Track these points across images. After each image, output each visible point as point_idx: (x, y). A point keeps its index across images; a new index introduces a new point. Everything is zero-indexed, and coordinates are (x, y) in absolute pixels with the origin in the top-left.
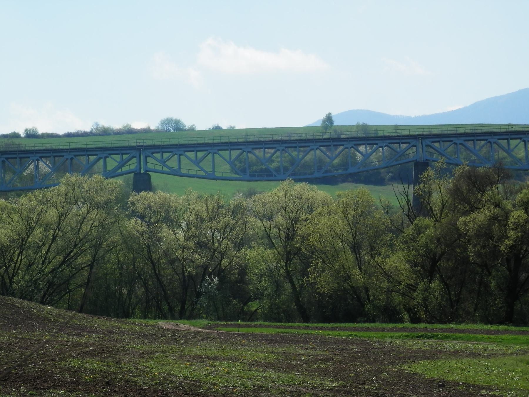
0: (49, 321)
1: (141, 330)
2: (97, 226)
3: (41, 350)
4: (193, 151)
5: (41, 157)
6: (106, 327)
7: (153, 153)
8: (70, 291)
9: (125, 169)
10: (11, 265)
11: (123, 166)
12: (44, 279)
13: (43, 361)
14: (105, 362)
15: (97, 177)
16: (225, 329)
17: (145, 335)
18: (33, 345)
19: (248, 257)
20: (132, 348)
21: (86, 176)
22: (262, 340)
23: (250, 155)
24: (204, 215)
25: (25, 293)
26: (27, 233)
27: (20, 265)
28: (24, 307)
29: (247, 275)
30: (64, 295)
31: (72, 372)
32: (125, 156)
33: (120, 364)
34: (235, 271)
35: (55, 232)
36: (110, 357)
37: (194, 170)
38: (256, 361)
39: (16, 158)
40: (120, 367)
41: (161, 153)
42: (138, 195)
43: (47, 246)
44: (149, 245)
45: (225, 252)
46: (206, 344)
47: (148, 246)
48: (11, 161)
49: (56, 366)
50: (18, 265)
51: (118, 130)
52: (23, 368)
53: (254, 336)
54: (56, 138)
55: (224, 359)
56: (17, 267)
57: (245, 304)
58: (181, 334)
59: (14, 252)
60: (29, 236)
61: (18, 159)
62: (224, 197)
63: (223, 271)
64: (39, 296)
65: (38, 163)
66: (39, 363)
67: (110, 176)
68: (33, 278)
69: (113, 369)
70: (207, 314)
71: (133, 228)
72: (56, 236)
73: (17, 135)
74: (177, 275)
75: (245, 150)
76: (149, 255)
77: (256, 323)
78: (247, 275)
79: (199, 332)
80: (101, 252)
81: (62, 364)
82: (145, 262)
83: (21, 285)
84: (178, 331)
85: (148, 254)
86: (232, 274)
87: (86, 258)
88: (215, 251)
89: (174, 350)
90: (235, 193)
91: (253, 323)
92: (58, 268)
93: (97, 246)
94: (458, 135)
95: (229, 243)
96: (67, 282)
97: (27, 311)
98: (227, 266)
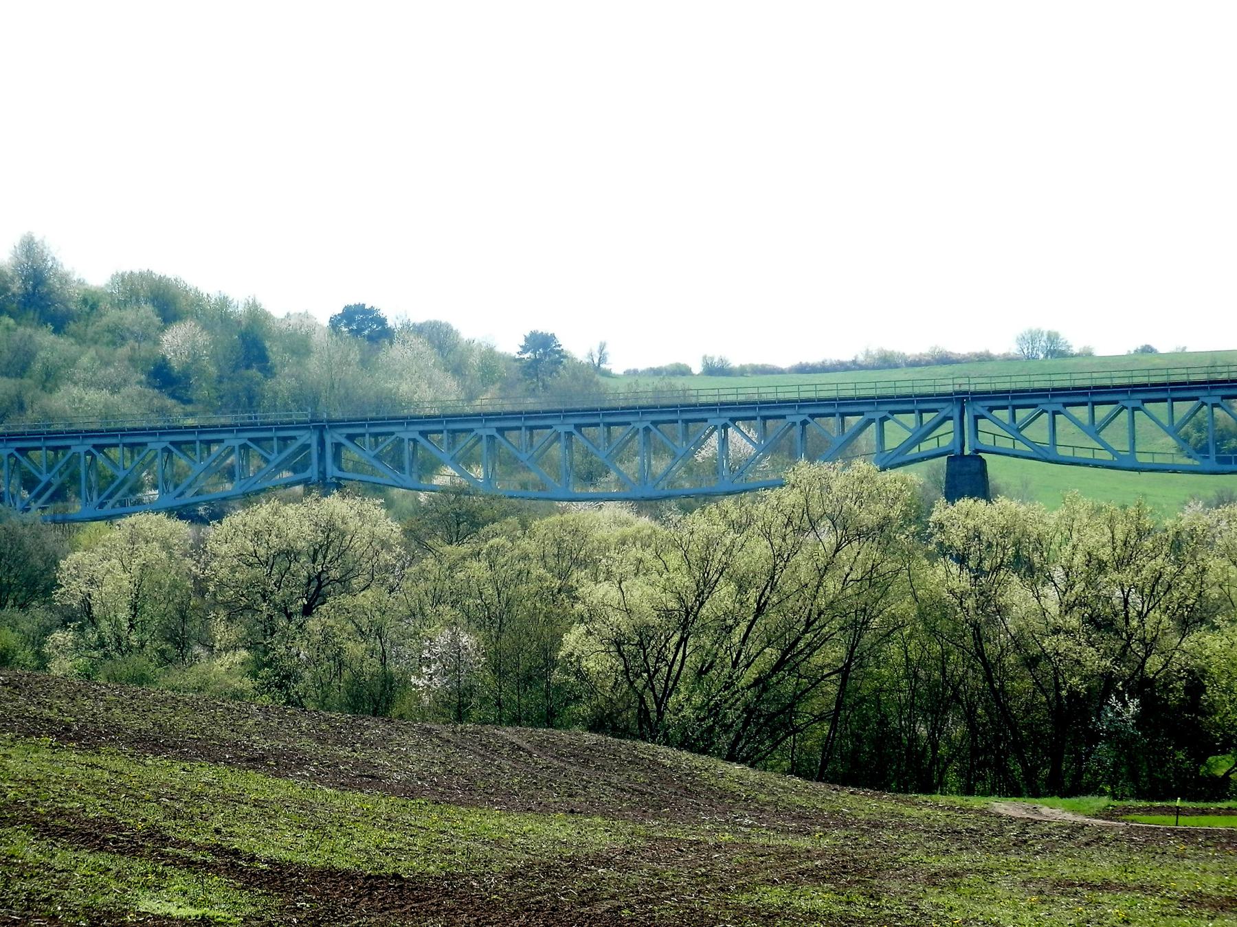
0: (736, 797)
1: (948, 820)
2: (858, 581)
3: (700, 866)
4: (1085, 404)
5: (734, 420)
6: (867, 814)
7: (991, 409)
8: (797, 730)
9: (928, 446)
10: (659, 668)
11: (923, 438)
12: (736, 701)
13: (699, 892)
14: (843, 895)
15: (862, 466)
16: (1146, 818)
17: (955, 832)
18: (684, 854)
19: (1208, 653)
20: (913, 862)
21: (839, 464)
22: (1228, 843)
23: (1216, 410)
24: (1105, 554)
25: (693, 734)
26: (699, 595)
27: (681, 668)
28: (680, 767)
29: (1206, 694)
30: (784, 738)
31: (763, 916)
32: (927, 417)
33: (879, 900)
34: (1179, 684)
35: (762, 594)
36: (858, 882)
37: (1086, 447)
38: (1199, 894)
39: (676, 422)
40: (875, 906)
41: (1010, 408)
42: (952, 507)
43: (743, 626)
44: (976, 622)
45: (1154, 639)
46: (1093, 853)
47: (976, 627)
48: (666, 427)
49: (727, 904)
50: (676, 668)
51: (916, 356)
52: (650, 907)
53: (1209, 834)
54: (774, 376)
55: (1124, 887)
56: (674, 674)
57: (1202, 760)
58: (1041, 829)
59: (667, 641)
60: (702, 604)
61: (680, 425)
62: (1151, 511)
63: (1150, 682)
64: (724, 741)
65: (726, 432)
66: (689, 895)
67: (890, 463)
68: (711, 700)
69: (860, 911)
70: (1113, 783)
71: (942, 583)
72: (766, 603)
73: (683, 369)
74: (1044, 691)
75: (1206, 400)
76: (979, 646)
77: (1219, 805)
78: (1206, 694)
79: (1083, 826)
80: (868, 638)
81: (743, 899)
82: (969, 662)
83: (683, 717)
84: (1036, 823)
85: (976, 644)
86: (1171, 690)
87: (833, 654)
88: (1130, 637)
89: (1012, 868)
90: (1186, 503)
91: (1213, 804)
92: (770, 676)
93: (858, 626)
94: (640, 410)
95: (1165, 618)
96: (790, 708)
97: (687, 775)
98: (1160, 671)
